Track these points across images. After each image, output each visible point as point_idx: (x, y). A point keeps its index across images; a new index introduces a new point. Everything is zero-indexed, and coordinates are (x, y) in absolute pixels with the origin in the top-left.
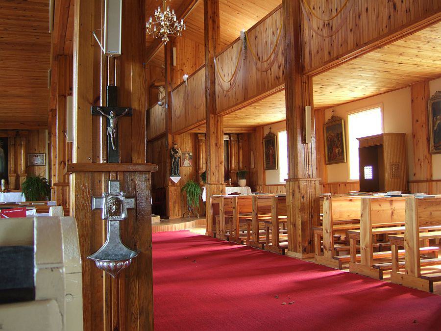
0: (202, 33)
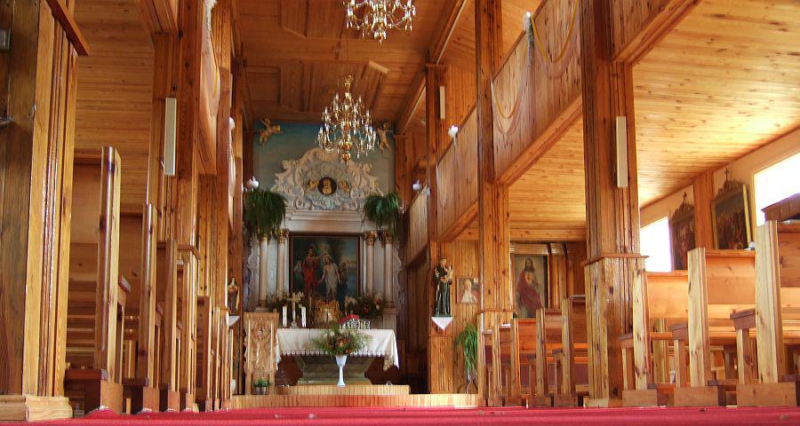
0: (471, 48)
